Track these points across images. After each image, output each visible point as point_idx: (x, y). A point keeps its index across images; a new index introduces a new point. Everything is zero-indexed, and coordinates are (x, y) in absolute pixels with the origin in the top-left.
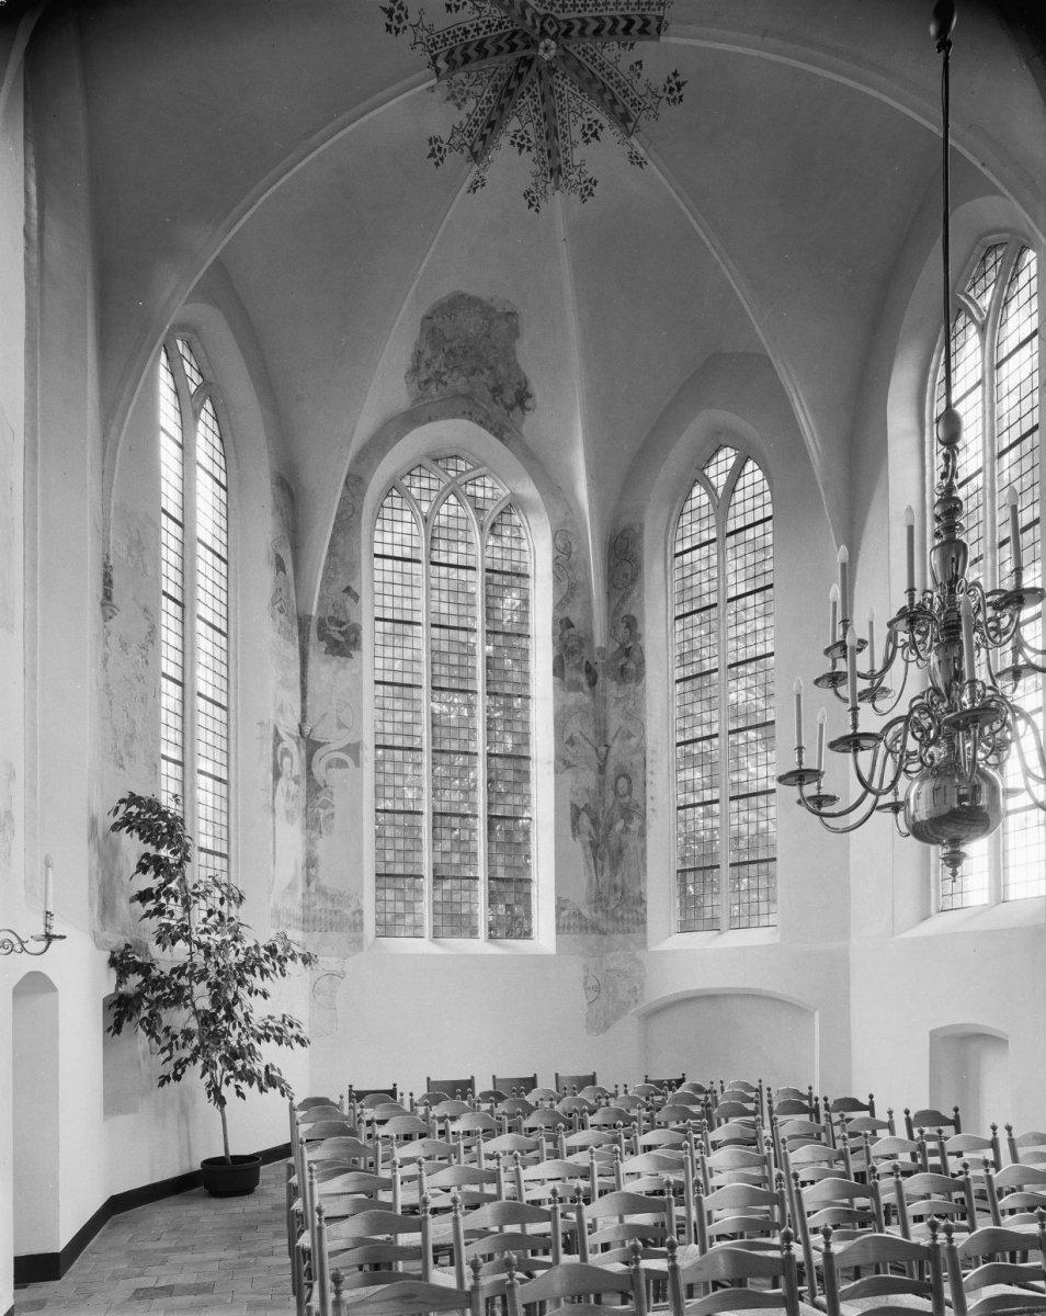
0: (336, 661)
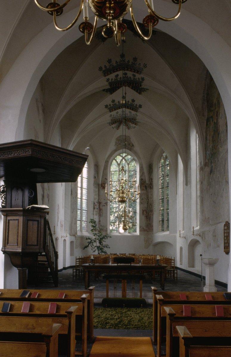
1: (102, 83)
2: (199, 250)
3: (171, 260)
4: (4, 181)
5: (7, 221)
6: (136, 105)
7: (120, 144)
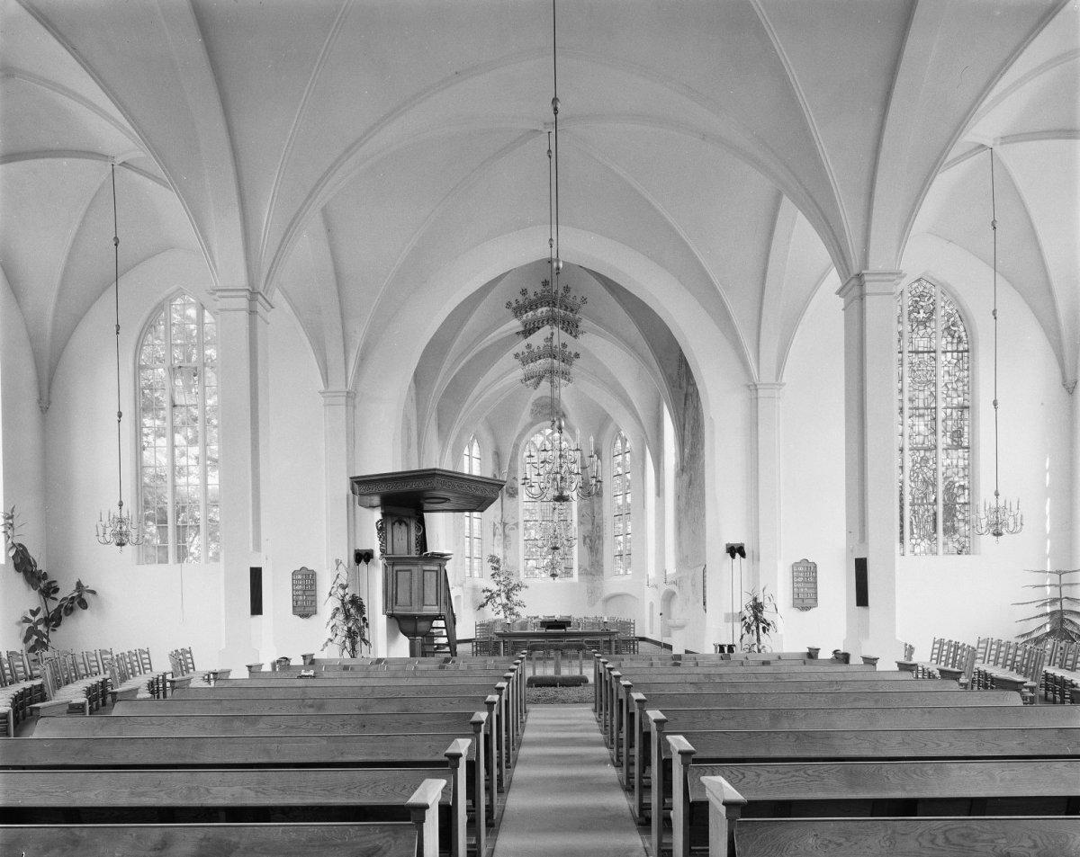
1: (515, 324)
3: (630, 623)
6: (570, 353)
7: (540, 412)
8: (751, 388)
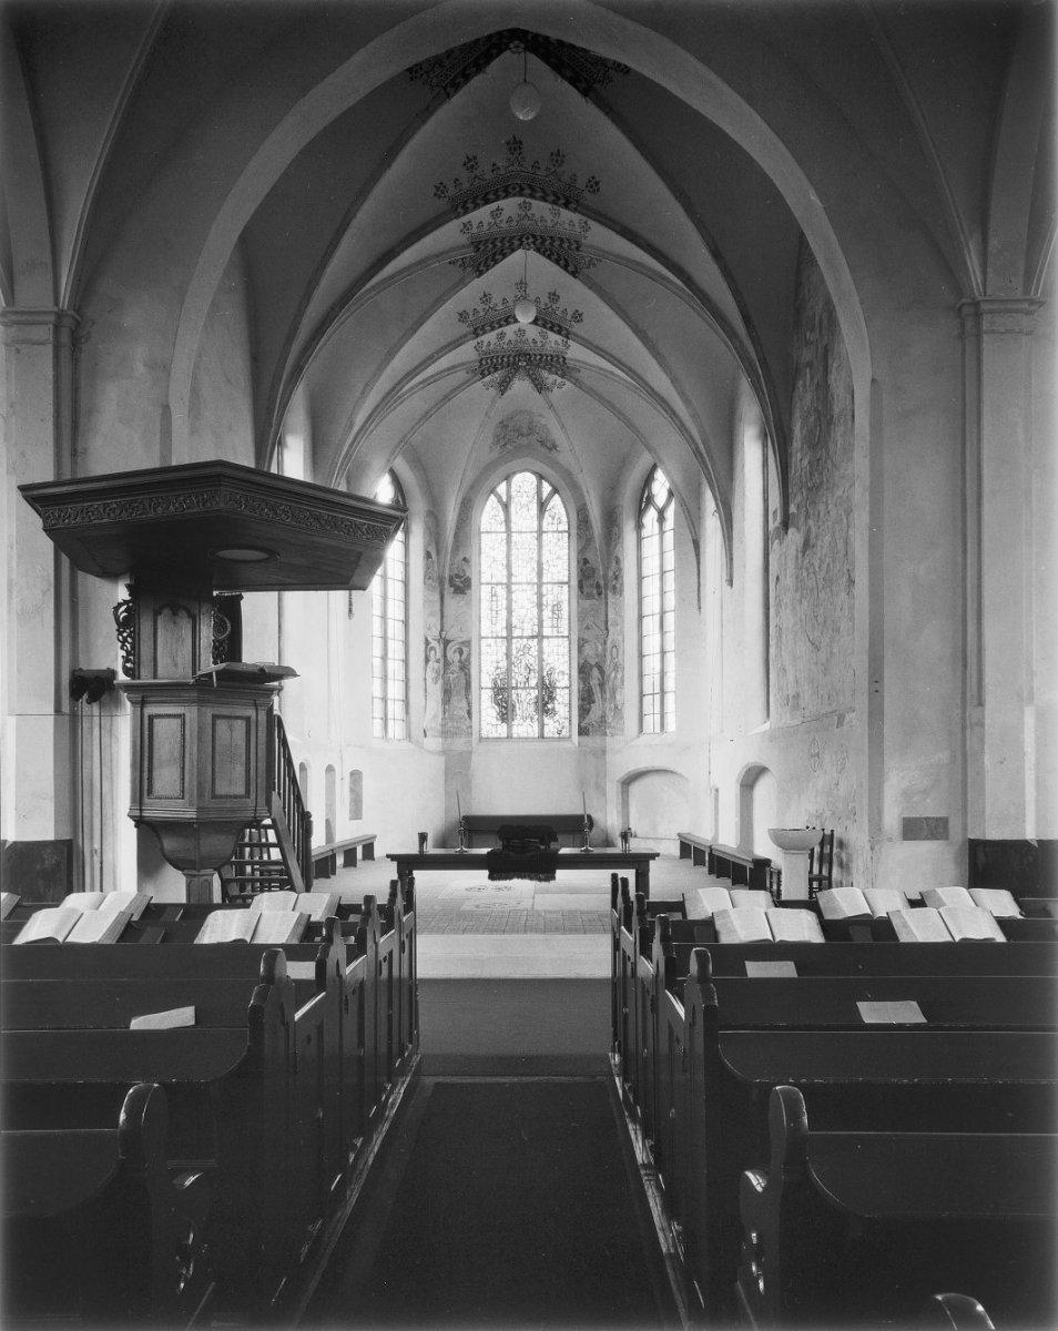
0: (459, 597)
2: (764, 790)
4: (128, 586)
5: (146, 722)
8: (966, 310)
